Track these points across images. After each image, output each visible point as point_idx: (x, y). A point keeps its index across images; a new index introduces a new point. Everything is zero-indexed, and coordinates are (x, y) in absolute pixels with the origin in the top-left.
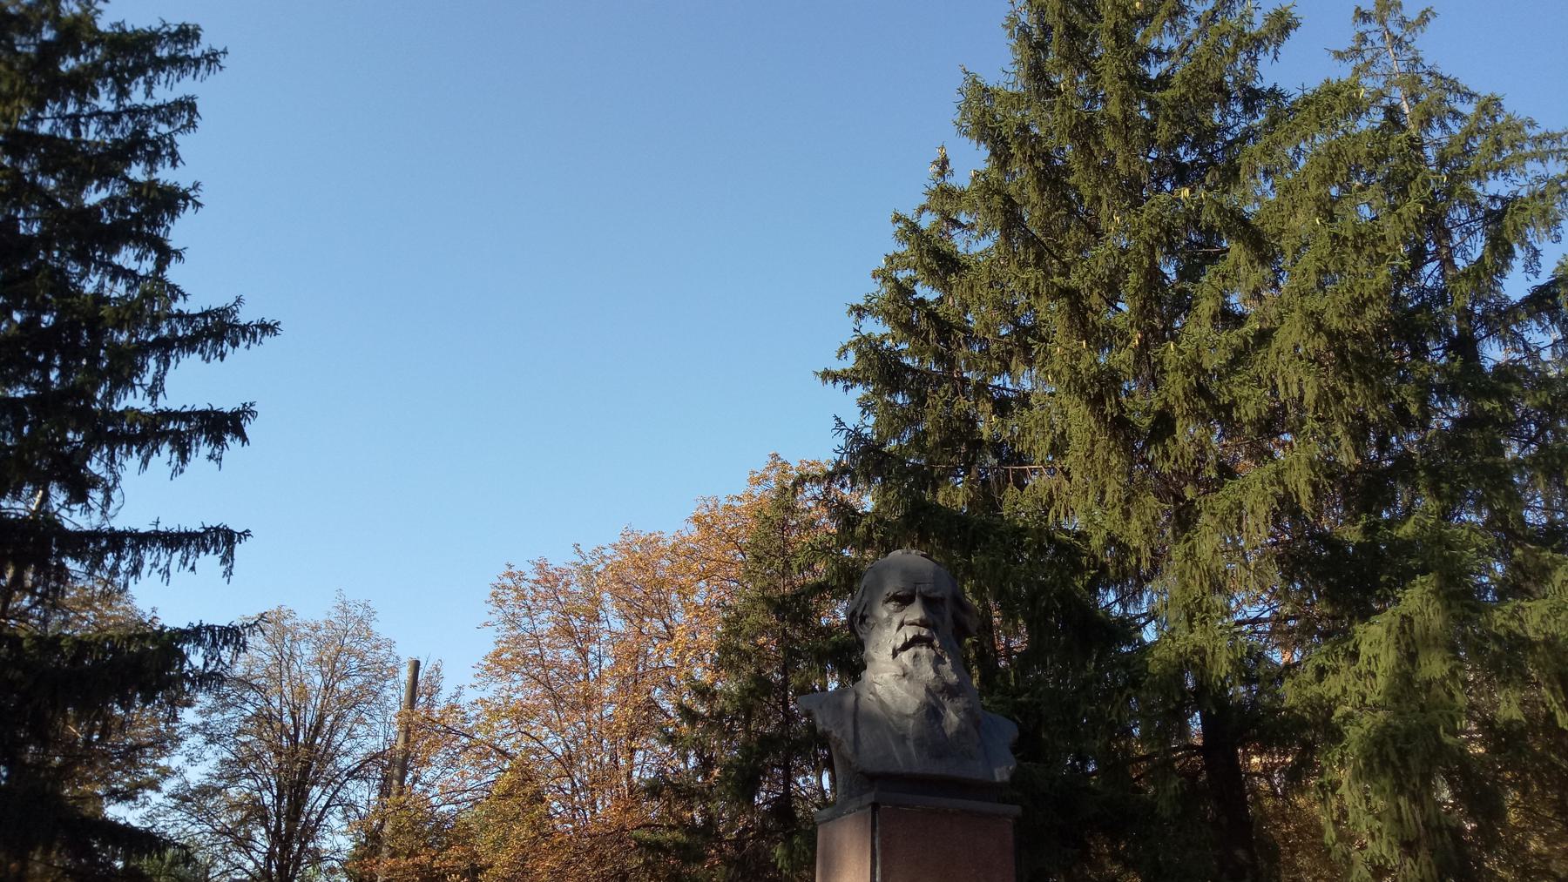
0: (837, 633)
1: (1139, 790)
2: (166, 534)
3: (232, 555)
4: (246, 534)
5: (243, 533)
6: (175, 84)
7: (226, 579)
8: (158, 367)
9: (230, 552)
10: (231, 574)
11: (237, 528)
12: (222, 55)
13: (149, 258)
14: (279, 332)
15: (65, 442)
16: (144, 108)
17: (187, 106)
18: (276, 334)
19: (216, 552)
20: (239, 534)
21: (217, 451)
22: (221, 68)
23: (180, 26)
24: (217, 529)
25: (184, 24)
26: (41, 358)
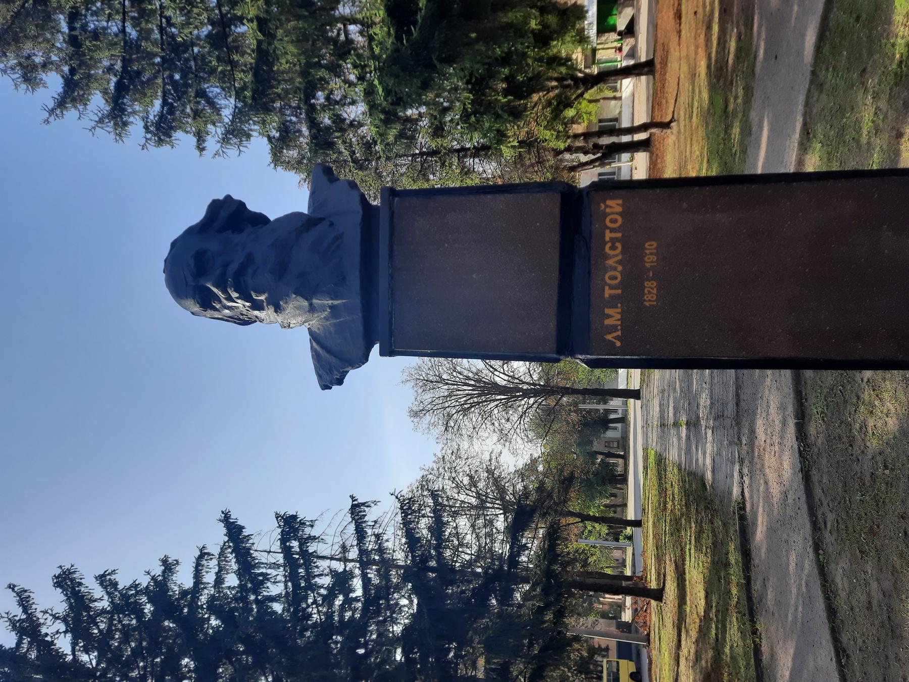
0: (564, 556)
1: (254, 637)
2: (358, 539)
3: (365, 503)
4: (352, 497)
5: (352, 499)
6: (89, 588)
7: (378, 503)
8: (262, 568)
9: (363, 504)
10: (375, 501)
11: (349, 503)
12: (63, 568)
13: (208, 564)
14: (227, 511)
15: (309, 637)
16: (110, 600)
17: (104, 580)
18: (229, 512)
19: (365, 511)
20: (353, 501)
21: (308, 523)
22: (72, 566)
23: (55, 587)
24: (352, 514)
25: (54, 586)
26: (405, 28)
